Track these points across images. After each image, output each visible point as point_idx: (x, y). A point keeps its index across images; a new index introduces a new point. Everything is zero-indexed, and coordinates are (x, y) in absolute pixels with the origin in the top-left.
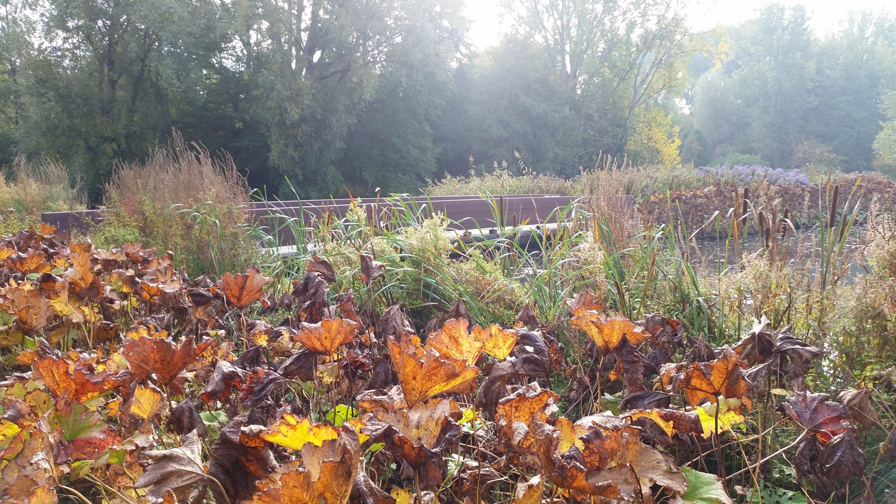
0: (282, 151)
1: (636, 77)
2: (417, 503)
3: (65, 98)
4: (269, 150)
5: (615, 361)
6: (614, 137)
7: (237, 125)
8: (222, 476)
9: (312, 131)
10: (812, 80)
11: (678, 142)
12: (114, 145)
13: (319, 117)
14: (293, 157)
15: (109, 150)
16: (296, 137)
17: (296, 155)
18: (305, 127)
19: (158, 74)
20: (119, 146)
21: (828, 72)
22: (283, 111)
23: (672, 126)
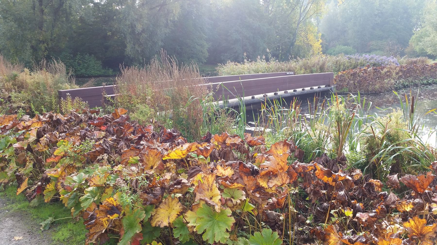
0: (132, 48)
1: (301, 8)
2: (1, 239)
3: (19, 20)
4: (125, 47)
5: (152, 168)
6: (289, 38)
7: (108, 34)
8: (291, 104)
9: (147, 37)
10: (377, 10)
11: (321, 41)
12: (45, 45)
13: (151, 29)
14: (138, 51)
15: (43, 48)
16: (139, 40)
17: (139, 50)
18: (144, 35)
19: (70, 7)
20: (48, 45)
21: (384, 5)
22: (133, 27)
23: (317, 33)
